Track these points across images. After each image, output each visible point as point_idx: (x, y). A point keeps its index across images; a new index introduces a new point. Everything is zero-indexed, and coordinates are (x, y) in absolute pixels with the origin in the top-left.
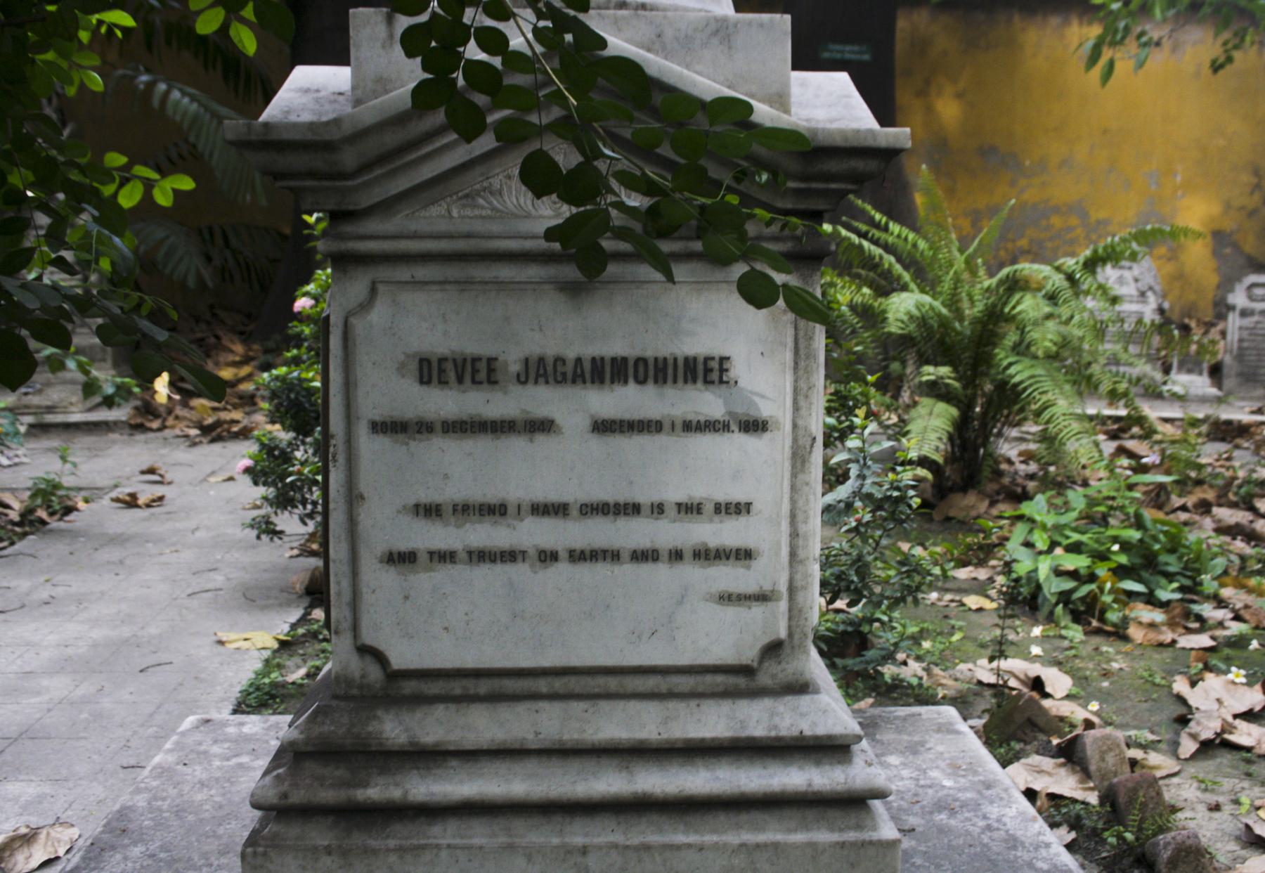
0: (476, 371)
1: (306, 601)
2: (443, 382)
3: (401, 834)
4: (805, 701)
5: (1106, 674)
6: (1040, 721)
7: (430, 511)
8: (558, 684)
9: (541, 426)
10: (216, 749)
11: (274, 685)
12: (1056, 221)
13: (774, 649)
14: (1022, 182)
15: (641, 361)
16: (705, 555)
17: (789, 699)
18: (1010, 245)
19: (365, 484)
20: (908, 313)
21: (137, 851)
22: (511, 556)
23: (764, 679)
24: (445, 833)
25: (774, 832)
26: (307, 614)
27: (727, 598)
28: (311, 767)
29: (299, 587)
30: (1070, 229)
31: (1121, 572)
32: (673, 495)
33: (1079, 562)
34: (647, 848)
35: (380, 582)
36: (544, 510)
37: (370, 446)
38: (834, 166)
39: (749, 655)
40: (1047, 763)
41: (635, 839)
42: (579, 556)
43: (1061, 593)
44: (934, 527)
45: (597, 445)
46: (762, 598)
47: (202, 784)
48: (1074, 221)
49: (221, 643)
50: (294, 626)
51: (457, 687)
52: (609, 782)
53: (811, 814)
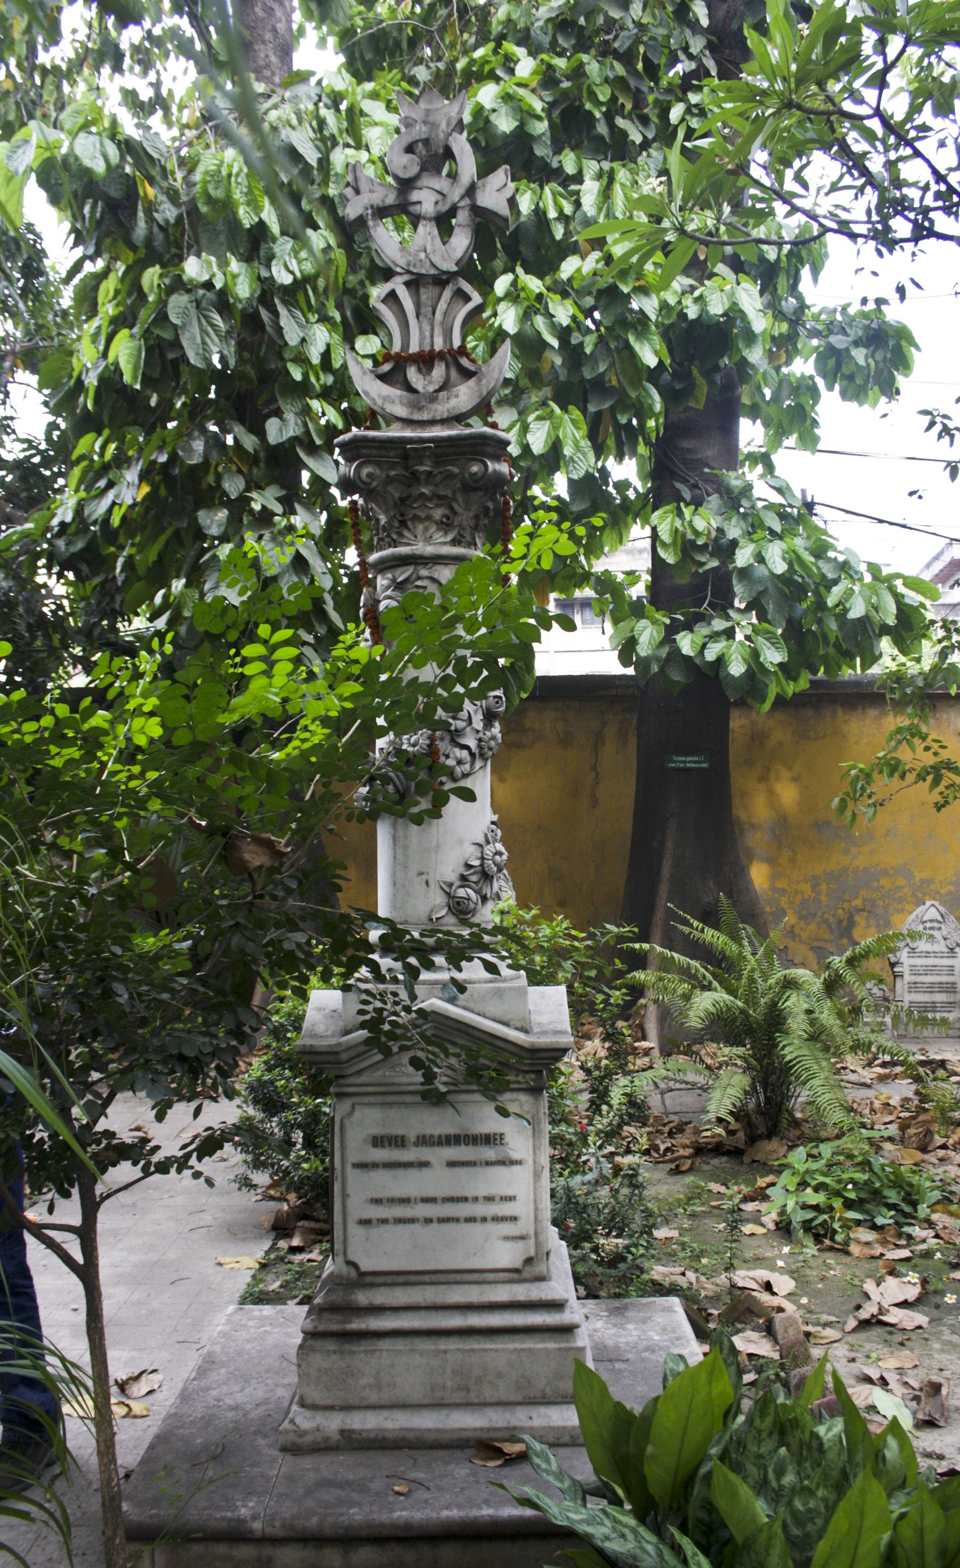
0: (399, 1142)
1: (273, 1235)
2: (383, 1146)
3: (365, 1345)
4: (543, 1285)
5: (823, 1279)
6: (755, 1309)
7: (378, 1201)
8: (434, 1278)
9: (424, 1164)
10: (250, 1323)
11: (261, 1292)
12: (885, 882)
14: (854, 850)
15: (466, 1136)
16: (497, 1219)
17: (537, 1284)
18: (846, 905)
19: (350, 1190)
20: (706, 1010)
21: (223, 1371)
22: (412, 1221)
23: (525, 1275)
24: (385, 1344)
25: (529, 1343)
26: (274, 1244)
27: (507, 1238)
28: (327, 1315)
29: (267, 1225)
30: (899, 888)
31: (849, 1205)
32: (482, 1193)
33: (819, 1198)
34: (473, 1350)
35: (356, 1231)
37: (351, 1173)
38: (542, 1055)
39: (518, 1264)
40: (754, 1335)
41: (468, 1347)
42: (442, 1220)
43: (804, 1222)
44: (743, 1169)
46: (522, 1238)
47: (248, 1341)
48: (901, 882)
49: (220, 1264)
50: (267, 1253)
51: (389, 1279)
53: (546, 1336)
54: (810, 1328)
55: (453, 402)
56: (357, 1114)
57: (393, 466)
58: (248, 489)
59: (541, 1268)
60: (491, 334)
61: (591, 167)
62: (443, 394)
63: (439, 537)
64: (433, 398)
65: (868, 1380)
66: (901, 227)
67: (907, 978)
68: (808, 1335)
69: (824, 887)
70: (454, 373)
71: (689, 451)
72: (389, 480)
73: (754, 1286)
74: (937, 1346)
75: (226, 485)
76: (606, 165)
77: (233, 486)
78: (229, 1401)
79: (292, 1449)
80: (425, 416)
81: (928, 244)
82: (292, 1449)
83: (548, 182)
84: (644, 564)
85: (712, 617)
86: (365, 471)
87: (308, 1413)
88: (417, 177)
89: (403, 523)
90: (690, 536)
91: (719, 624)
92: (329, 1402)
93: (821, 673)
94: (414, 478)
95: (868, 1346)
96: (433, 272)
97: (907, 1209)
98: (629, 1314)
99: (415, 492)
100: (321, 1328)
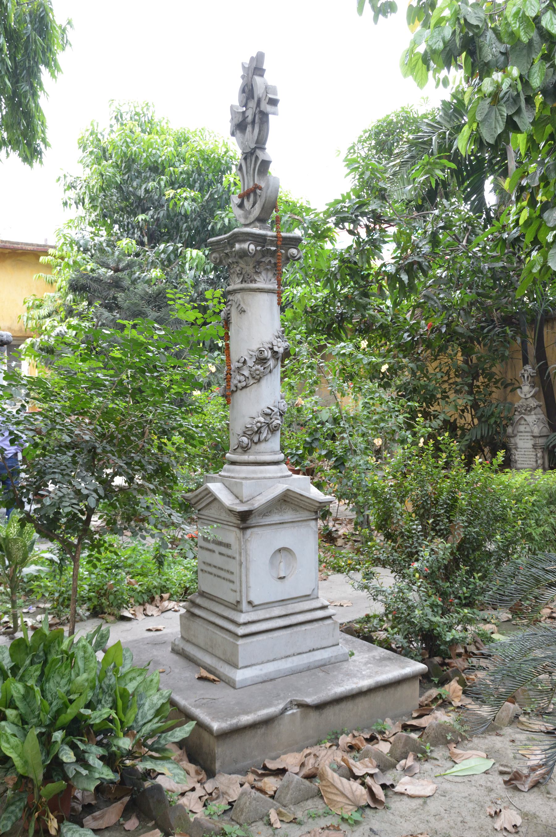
9: (214, 551)
13: (238, 602)
22: (219, 577)
24: (198, 620)
39: (234, 602)
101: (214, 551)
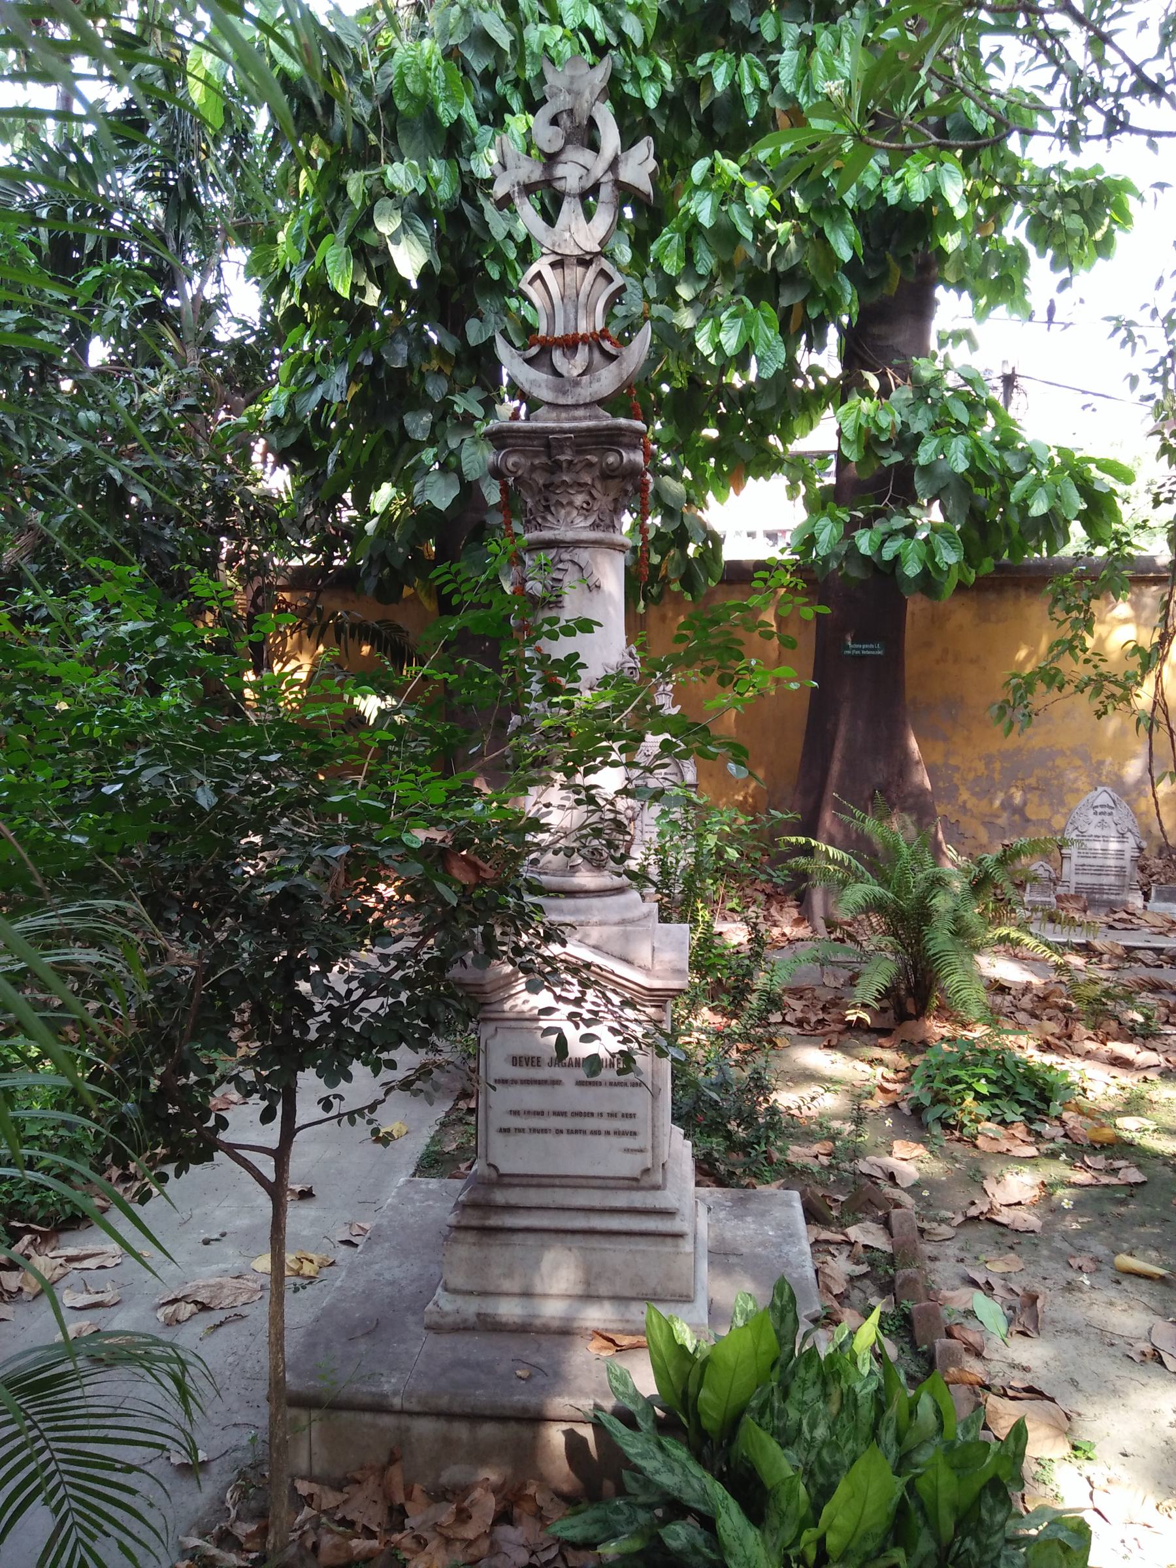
3: (502, 1237)
7: (516, 1113)
9: (556, 1083)
13: (646, 1171)
16: (618, 1133)
22: (545, 1131)
24: (518, 1238)
27: (627, 1150)
35: (497, 1140)
36: (558, 1114)
39: (636, 1173)
42: (570, 1132)
45: (578, 1089)
50: (448, 1114)
51: (525, 1181)
52: (580, 1222)
54: (925, 1225)
55: (596, 386)
56: (499, 1037)
57: (536, 454)
58: (451, 392)
59: (658, 1178)
60: (686, 225)
61: (792, 32)
62: (585, 379)
63: (581, 522)
64: (576, 383)
65: (974, 1283)
66: (1095, 122)
67: (1075, 860)
68: (922, 1231)
69: (998, 765)
70: (597, 355)
71: (880, 337)
72: (533, 468)
73: (879, 1174)
74: (1045, 1252)
75: (430, 389)
76: (808, 28)
77: (436, 389)
78: (388, 1276)
79: (435, 1328)
80: (570, 401)
81: (1124, 138)
82: (435, 1328)
83: (746, 50)
84: (832, 444)
85: (893, 514)
86: (511, 460)
87: (450, 1297)
88: (561, 151)
89: (547, 508)
90: (874, 431)
91: (899, 522)
92: (469, 1288)
93: (1005, 556)
94: (556, 467)
95: (978, 1247)
96: (577, 252)
97: (1040, 1105)
98: (752, 1206)
99: (557, 479)
100: (464, 1223)
101: (556, 1083)
